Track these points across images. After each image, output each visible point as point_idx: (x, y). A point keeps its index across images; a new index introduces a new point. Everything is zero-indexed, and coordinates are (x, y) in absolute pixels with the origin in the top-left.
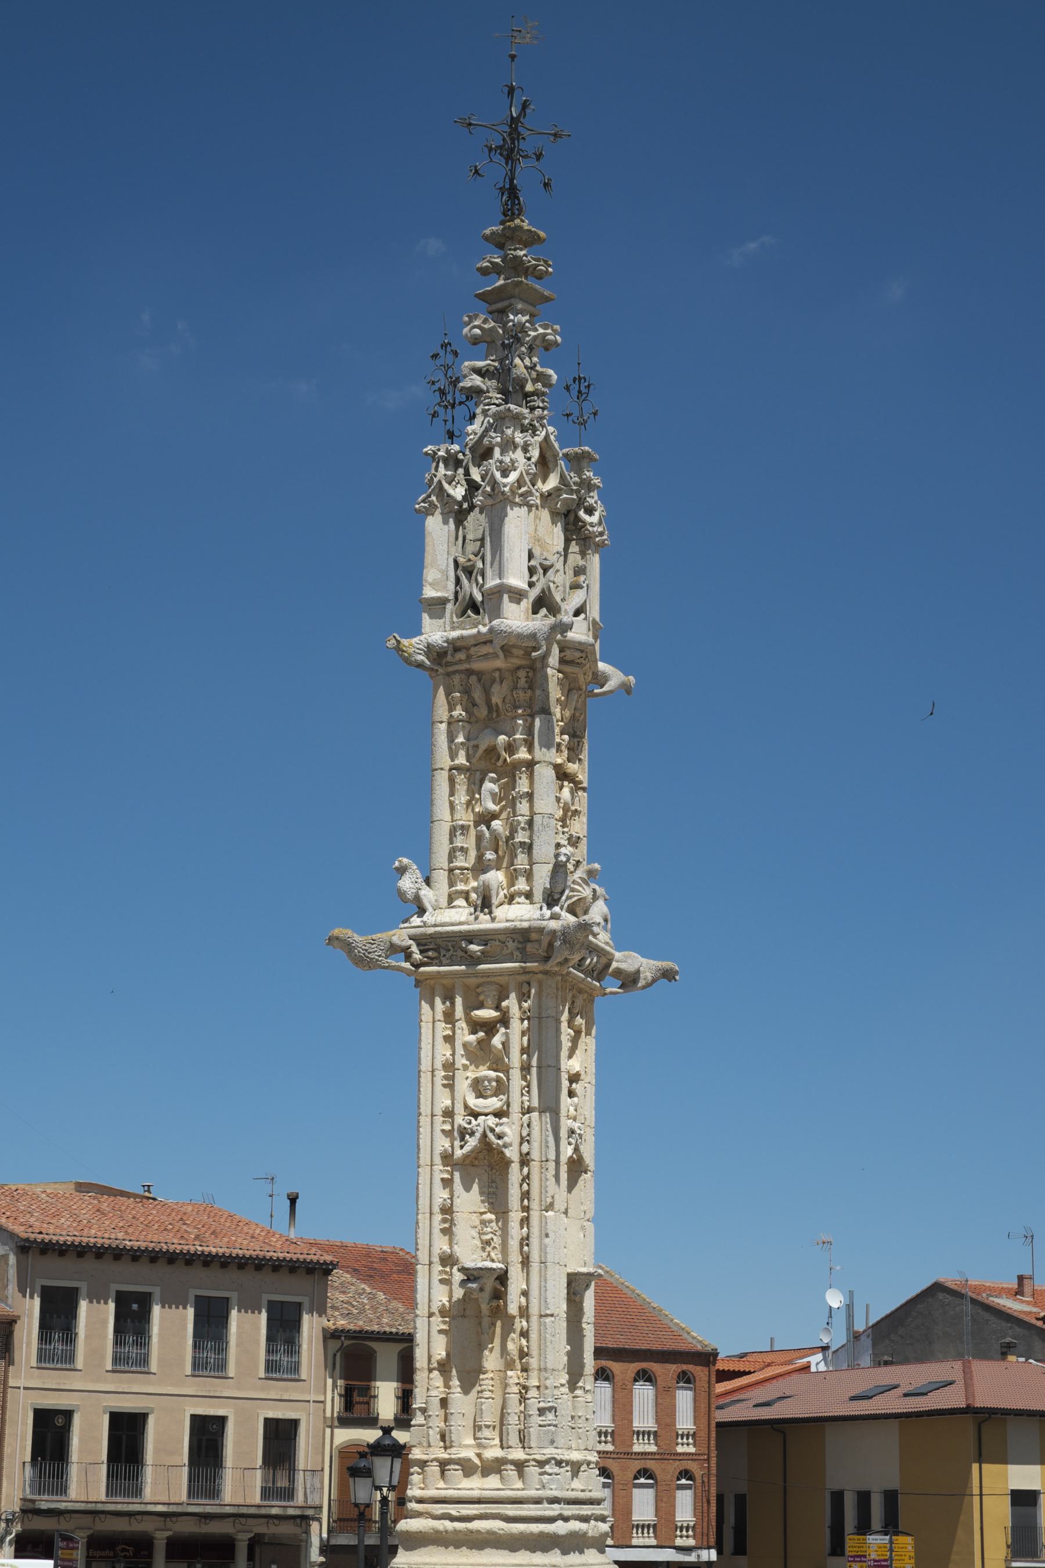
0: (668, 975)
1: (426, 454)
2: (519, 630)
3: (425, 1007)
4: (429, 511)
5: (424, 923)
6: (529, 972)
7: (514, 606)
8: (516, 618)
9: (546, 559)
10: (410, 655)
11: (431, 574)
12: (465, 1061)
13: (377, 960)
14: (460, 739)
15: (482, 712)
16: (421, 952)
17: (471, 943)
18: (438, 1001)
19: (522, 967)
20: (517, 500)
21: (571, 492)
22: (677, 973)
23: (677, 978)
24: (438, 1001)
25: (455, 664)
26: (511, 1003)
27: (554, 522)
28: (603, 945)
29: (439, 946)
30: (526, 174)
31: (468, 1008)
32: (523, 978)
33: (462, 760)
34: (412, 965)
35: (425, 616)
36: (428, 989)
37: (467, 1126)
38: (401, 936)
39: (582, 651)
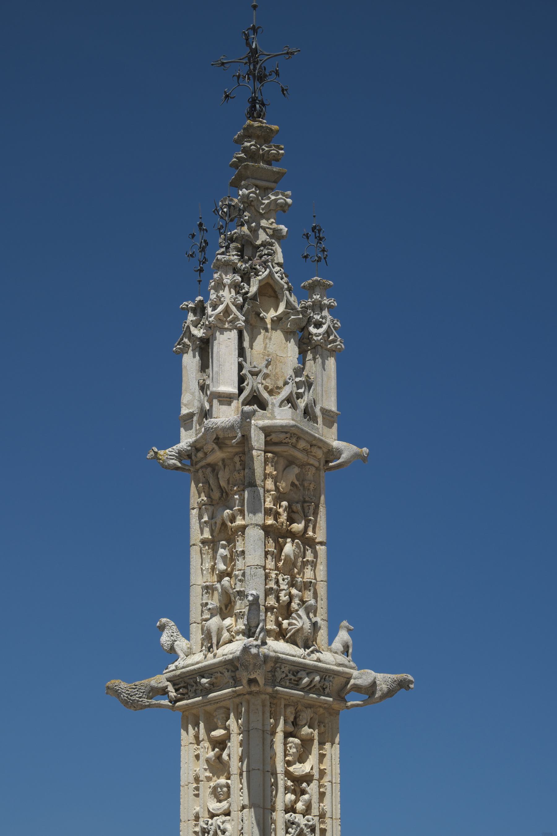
0: (403, 685)
1: (182, 308)
2: (223, 425)
3: (183, 732)
4: (184, 350)
5: (176, 666)
6: (239, 695)
7: (224, 408)
8: (225, 416)
9: (255, 367)
10: (164, 461)
11: (186, 398)
12: (208, 774)
13: (138, 701)
14: (206, 518)
15: (216, 495)
16: (177, 690)
17: (204, 677)
18: (190, 727)
19: (233, 691)
20: (226, 326)
21: (298, 313)
22: (411, 682)
23: (412, 686)
24: (190, 727)
25: (200, 461)
26: (232, 722)
27: (287, 340)
28: (335, 668)
29: (186, 683)
30: (269, 91)
31: (209, 730)
32: (237, 700)
33: (207, 535)
34: (170, 702)
35: (182, 430)
36: (191, 718)
37: (205, 826)
38: (160, 680)
39: (286, 433)
